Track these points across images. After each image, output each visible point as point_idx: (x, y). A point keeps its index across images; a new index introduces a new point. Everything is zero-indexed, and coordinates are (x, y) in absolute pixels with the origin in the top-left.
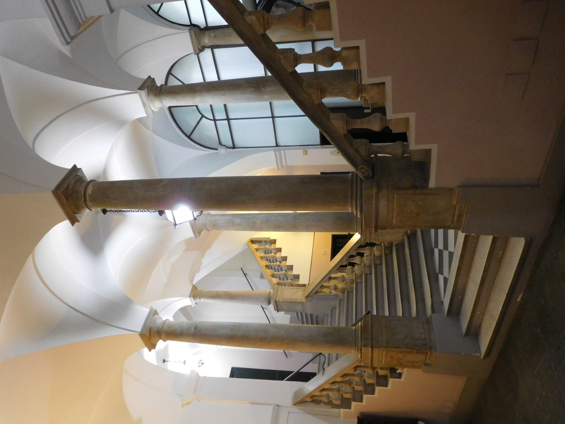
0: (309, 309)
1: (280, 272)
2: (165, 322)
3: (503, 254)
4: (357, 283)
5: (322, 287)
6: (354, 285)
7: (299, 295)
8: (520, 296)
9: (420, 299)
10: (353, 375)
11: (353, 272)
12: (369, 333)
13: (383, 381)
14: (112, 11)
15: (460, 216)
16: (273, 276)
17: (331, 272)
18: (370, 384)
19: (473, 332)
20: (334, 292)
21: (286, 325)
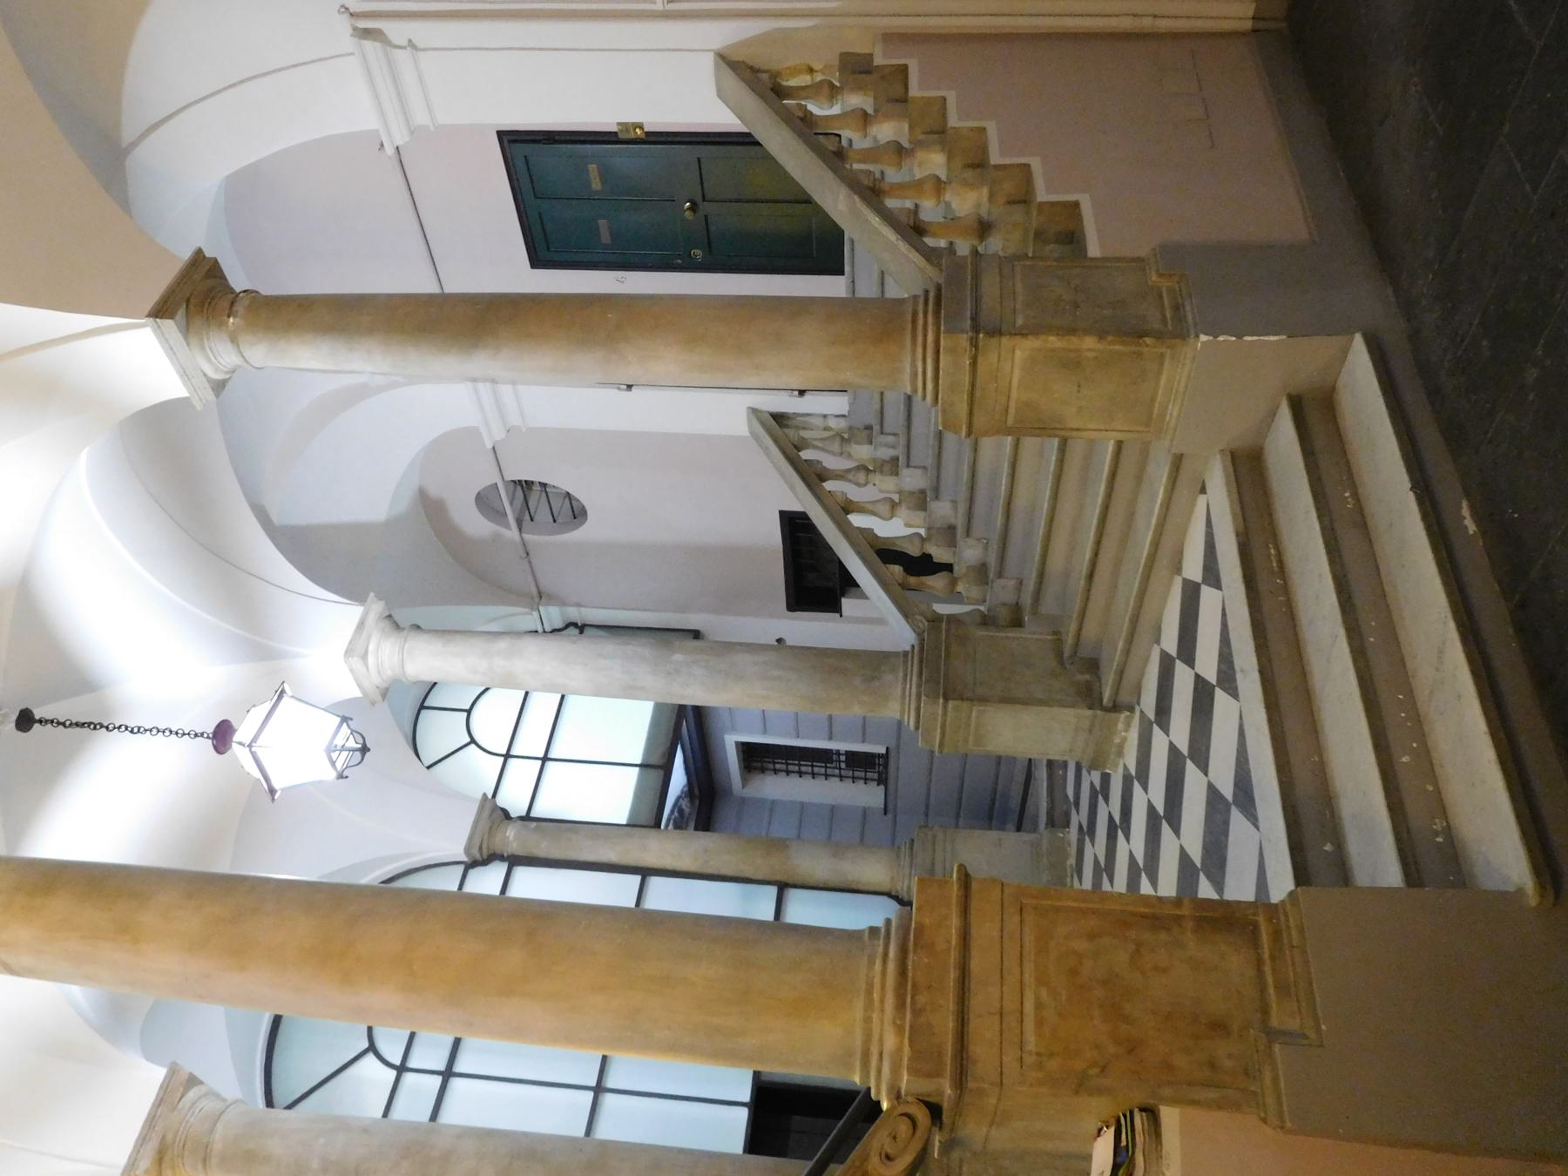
3: (1356, 495)
8: (1465, 512)
14: (390, 616)
15: (1177, 308)
19: (1431, 855)
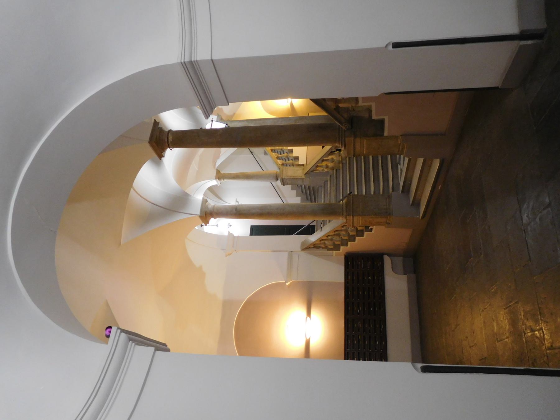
0: (307, 183)
1: (282, 155)
2: (214, 206)
4: (342, 164)
5: (317, 166)
6: (341, 165)
7: (299, 173)
9: (386, 180)
10: (341, 230)
11: (339, 156)
12: (351, 206)
13: (360, 233)
15: (403, 149)
16: (278, 158)
17: (323, 157)
18: (352, 235)
19: (416, 203)
20: (326, 170)
21: (298, 204)
